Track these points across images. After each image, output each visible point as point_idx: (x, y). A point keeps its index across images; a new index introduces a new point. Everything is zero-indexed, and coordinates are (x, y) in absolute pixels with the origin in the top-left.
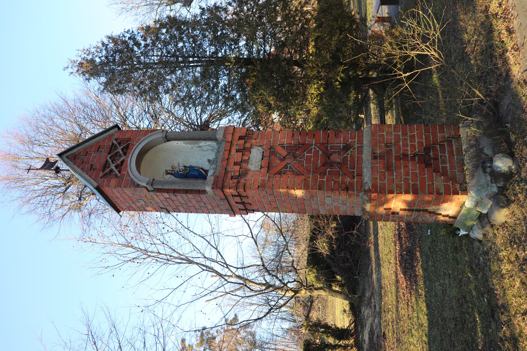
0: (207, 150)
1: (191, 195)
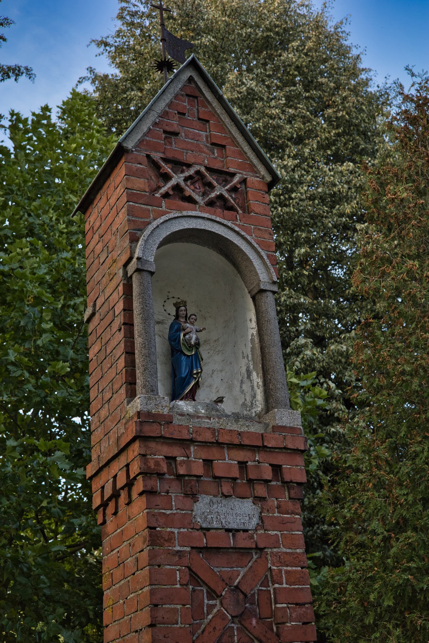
0: (242, 392)
1: (123, 364)
